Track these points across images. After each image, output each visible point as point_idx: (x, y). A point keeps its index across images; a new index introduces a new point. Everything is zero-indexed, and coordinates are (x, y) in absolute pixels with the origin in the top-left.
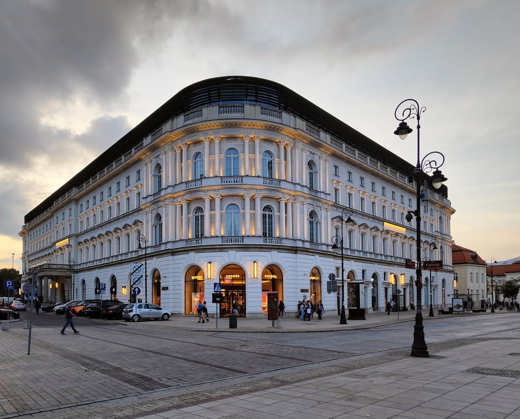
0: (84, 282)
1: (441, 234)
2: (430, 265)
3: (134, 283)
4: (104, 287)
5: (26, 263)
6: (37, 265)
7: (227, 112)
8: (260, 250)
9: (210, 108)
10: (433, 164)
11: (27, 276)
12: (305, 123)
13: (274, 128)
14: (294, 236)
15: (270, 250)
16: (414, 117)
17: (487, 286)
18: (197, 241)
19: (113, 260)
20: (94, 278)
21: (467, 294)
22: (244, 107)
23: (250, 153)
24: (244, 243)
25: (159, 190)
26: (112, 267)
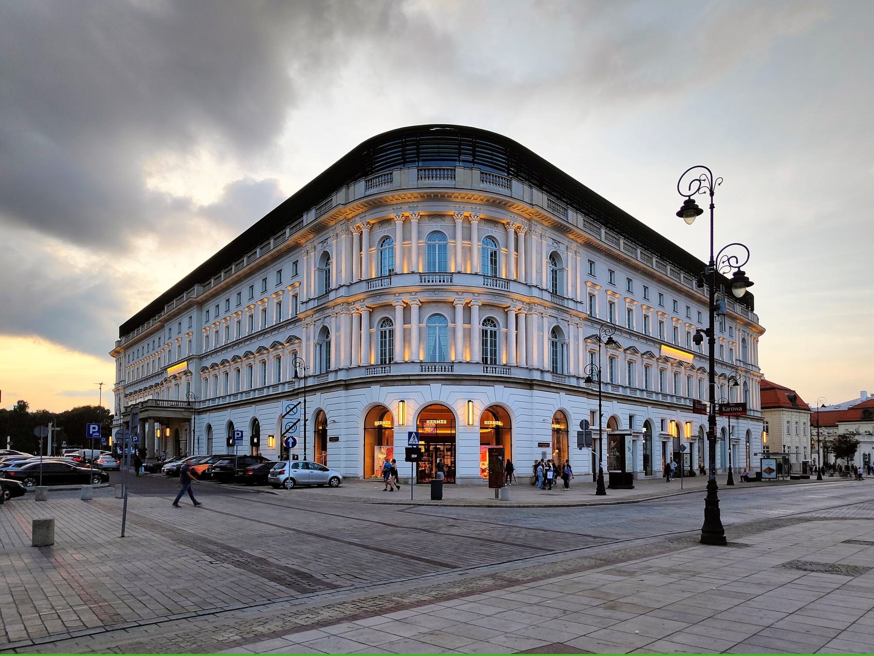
0: (209, 427)
1: (745, 363)
2: (728, 409)
3: (287, 431)
4: (240, 436)
5: (120, 398)
7: (431, 178)
9: (405, 171)
10: (733, 262)
11: (122, 417)
12: (545, 197)
13: (500, 203)
15: (492, 384)
16: (705, 193)
17: (811, 440)
20: (249, 420)
21: (783, 452)
22: (455, 170)
23: (463, 239)
25: (326, 291)
26: (254, 406)
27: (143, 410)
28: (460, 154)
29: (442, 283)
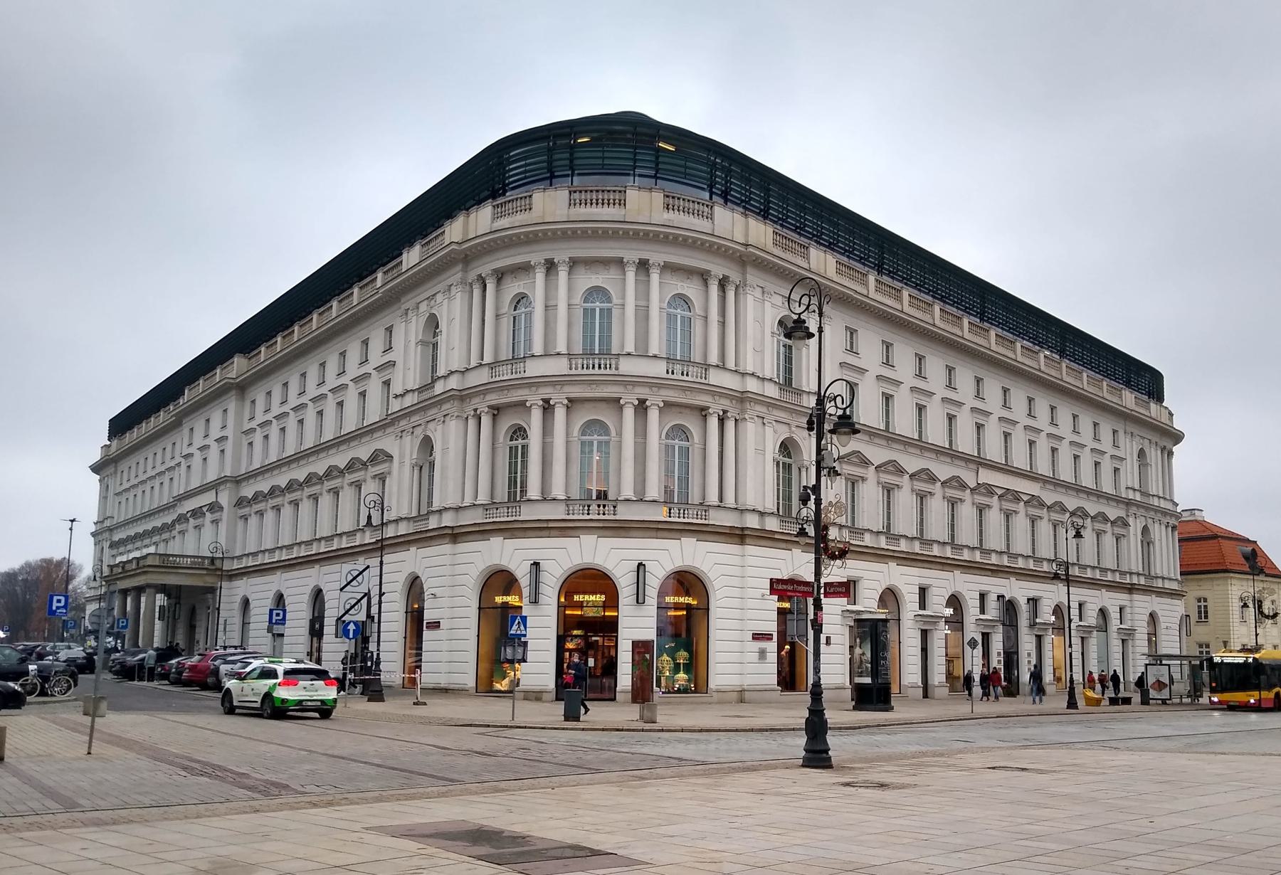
0: (246, 603)
4: (281, 617)
5: (103, 548)
6: (131, 556)
8: (655, 536)
9: (551, 193)
11: (104, 583)
12: (770, 230)
14: (740, 502)
15: (677, 535)
18: (586, 508)
19: (281, 557)
20: (308, 591)
22: (625, 192)
24: (617, 517)
25: (432, 377)
26: (317, 567)
27: (138, 571)
28: (635, 168)
29: (596, 371)
